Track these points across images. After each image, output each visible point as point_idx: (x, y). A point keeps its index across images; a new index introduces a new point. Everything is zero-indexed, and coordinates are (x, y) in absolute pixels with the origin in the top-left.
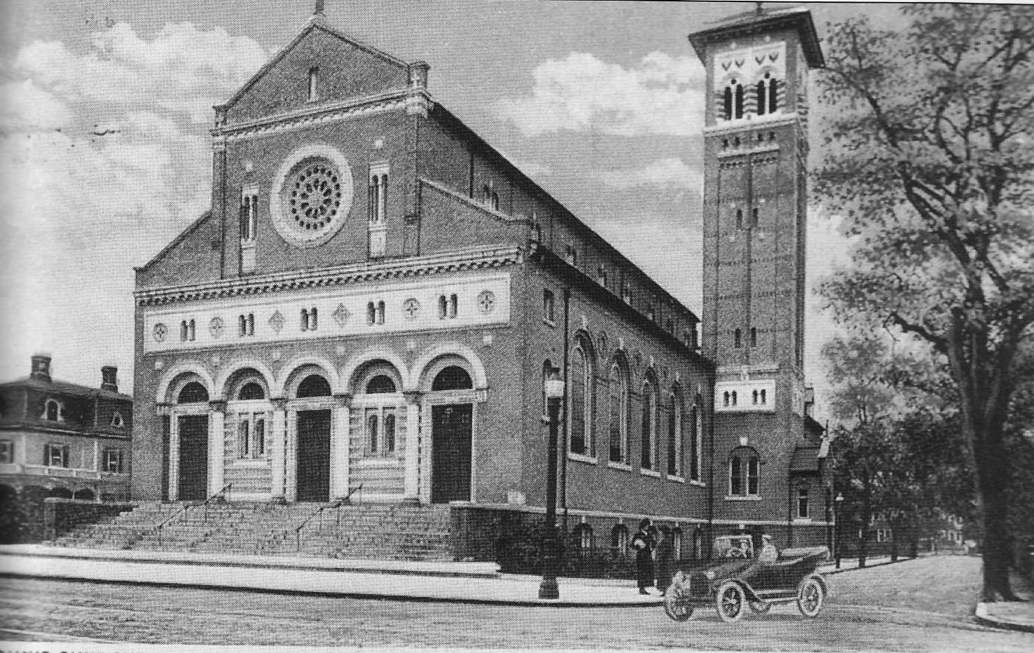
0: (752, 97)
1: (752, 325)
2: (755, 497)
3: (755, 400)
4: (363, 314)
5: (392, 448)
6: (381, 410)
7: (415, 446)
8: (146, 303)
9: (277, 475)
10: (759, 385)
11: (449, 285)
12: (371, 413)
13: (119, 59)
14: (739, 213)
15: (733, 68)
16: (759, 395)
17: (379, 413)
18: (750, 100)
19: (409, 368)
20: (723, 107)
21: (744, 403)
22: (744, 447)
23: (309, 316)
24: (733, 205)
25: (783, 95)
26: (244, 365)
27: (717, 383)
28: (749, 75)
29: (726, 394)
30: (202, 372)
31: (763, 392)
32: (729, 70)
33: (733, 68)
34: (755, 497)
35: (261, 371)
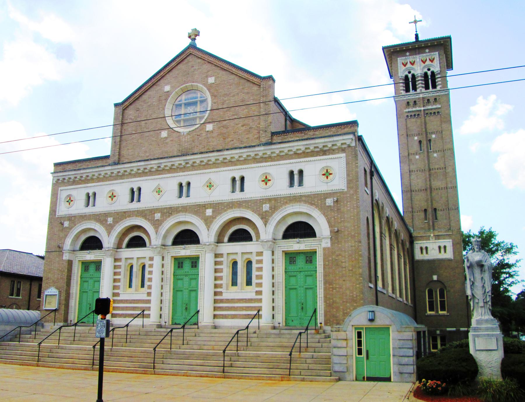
0: (421, 80)
1: (435, 206)
2: (444, 313)
3: (440, 252)
4: (127, 196)
5: (143, 286)
6: (135, 260)
7: (159, 283)
8: (57, 184)
9: (154, 306)
10: (442, 242)
11: (136, 182)
12: (130, 261)
13: (416, 32)
14: (420, 142)
15: (409, 65)
16: (442, 249)
17: (134, 262)
18: (420, 84)
19: (109, 233)
20: (424, 86)
21: (434, 254)
22: (435, 281)
23: (90, 199)
24: (416, 138)
25: (440, 83)
26: (241, 228)
27: (415, 242)
28: (418, 70)
29: (421, 249)
30: (101, 233)
31: (445, 247)
32: (407, 66)
33: (409, 65)
34: (444, 313)
35: (150, 233)
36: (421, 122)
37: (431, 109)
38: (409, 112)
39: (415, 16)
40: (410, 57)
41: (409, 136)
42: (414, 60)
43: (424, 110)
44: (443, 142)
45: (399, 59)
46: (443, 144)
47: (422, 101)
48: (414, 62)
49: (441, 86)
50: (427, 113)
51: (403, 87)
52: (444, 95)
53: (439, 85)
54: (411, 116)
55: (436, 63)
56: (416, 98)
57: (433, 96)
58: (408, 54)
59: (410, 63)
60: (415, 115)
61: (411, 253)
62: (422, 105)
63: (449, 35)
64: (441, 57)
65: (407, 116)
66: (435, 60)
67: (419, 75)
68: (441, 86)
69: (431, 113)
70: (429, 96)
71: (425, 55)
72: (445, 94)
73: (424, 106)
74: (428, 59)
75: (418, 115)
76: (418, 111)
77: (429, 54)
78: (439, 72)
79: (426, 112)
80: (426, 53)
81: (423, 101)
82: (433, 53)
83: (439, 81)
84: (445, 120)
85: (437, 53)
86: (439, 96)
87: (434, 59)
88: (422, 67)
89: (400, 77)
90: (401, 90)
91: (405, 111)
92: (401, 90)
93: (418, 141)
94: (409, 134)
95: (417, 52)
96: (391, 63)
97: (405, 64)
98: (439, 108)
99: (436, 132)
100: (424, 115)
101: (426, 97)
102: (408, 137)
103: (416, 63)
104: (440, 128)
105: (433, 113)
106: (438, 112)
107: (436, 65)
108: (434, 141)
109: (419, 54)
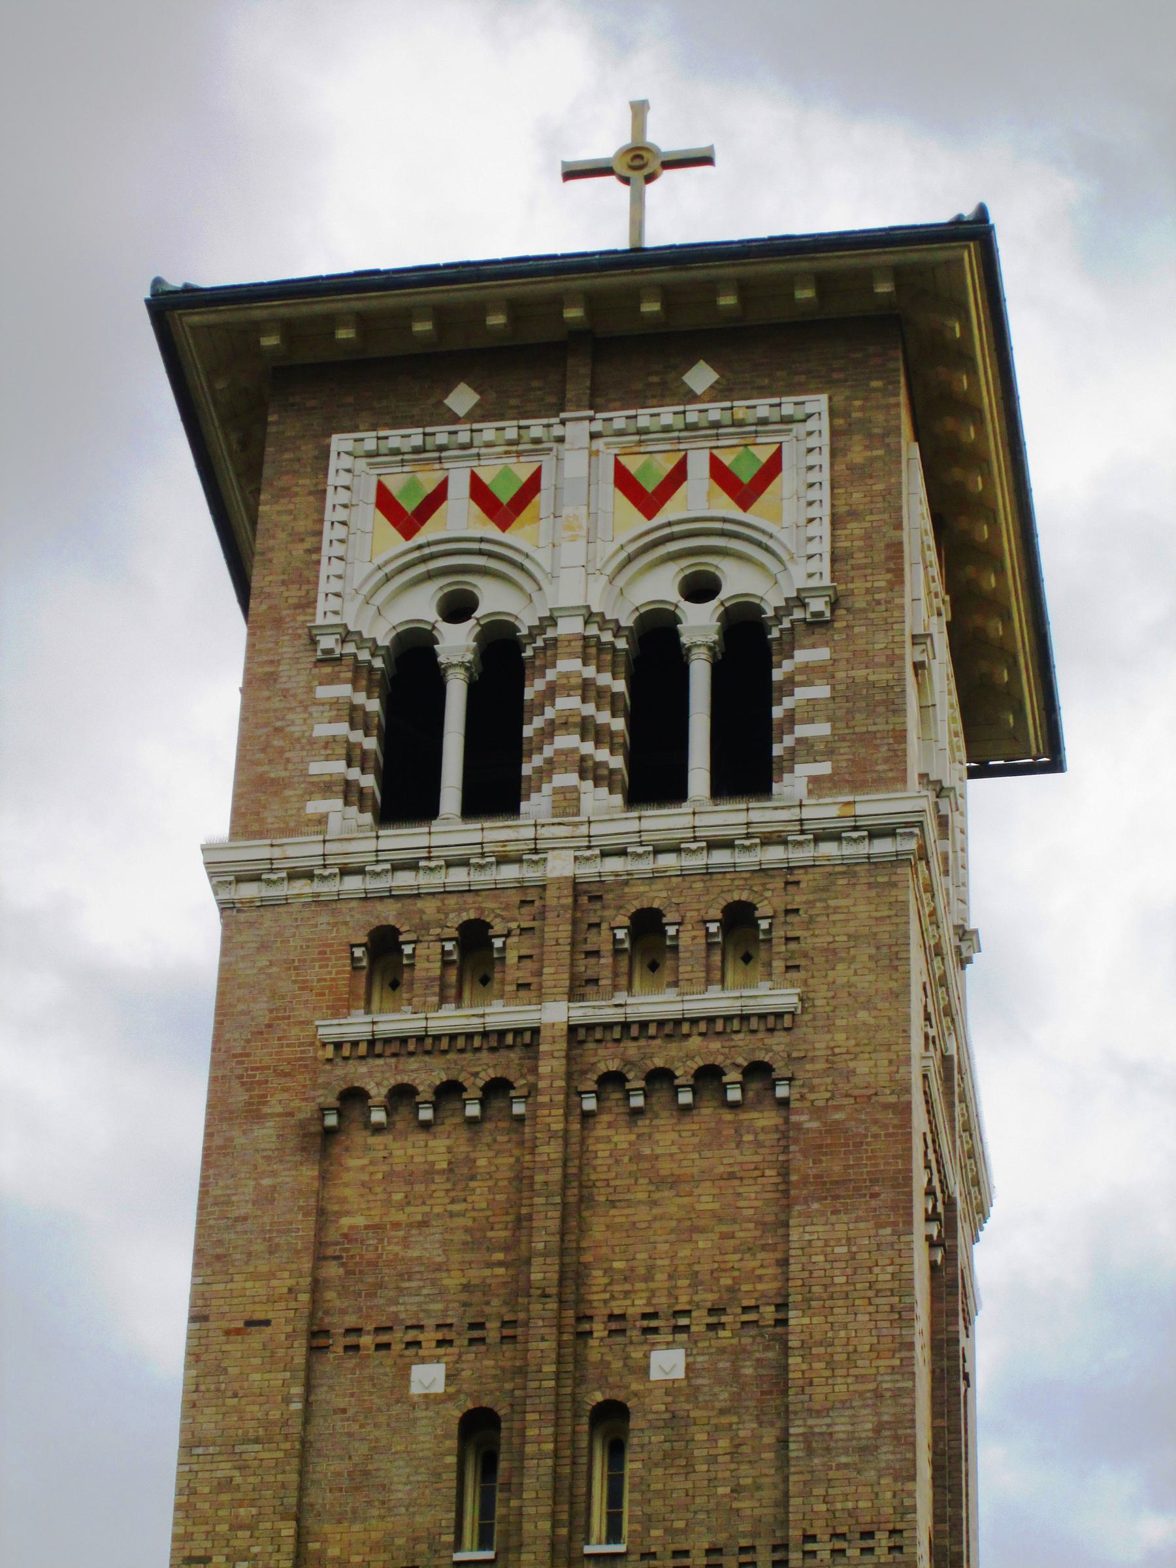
25: (822, 729)
36: (522, 1179)
37: (671, 1029)
38: (375, 1047)
39: (572, 173)
40: (489, 431)
41: (338, 1343)
42: (524, 473)
43: (575, 1033)
44: (783, 1441)
45: (339, 442)
46: (783, 1461)
47: (559, 931)
48: (532, 486)
49: (824, 768)
50: (613, 1080)
51: (355, 716)
52: (849, 868)
53: (807, 750)
54: (402, 1095)
55: (792, 512)
56: (497, 890)
57: (707, 873)
58: (462, 399)
59: (480, 492)
60: (450, 1091)
61: (299, 1526)
62: (556, 975)
63: (968, 211)
64: (858, 454)
65: (354, 1097)
66: (786, 483)
67: (569, 627)
68: (824, 768)
69: (660, 1077)
70: (656, 876)
71: (667, 415)
72: (869, 860)
73: (574, 995)
74: (699, 466)
75: (497, 1088)
76: (496, 1039)
77: (715, 411)
78: (818, 605)
79: (607, 1060)
80: (691, 397)
81: (582, 927)
82: (763, 407)
83: (811, 673)
84: (834, 1167)
85: (818, 403)
86: (789, 875)
87: (773, 467)
88: (608, 550)
89: (327, 642)
90: (325, 788)
91: (330, 1029)
92: (325, 788)
93: (455, 1413)
94: (338, 1323)
95: (577, 387)
96: (252, 473)
97: (410, 505)
98: (773, 1021)
99: (699, 1321)
100: (573, 1093)
101: (625, 881)
102: (327, 1364)
103: (543, 499)
104: (762, 1263)
105: (683, 1072)
106: (758, 1071)
107: (784, 537)
108: (674, 1421)
109: (596, 400)
